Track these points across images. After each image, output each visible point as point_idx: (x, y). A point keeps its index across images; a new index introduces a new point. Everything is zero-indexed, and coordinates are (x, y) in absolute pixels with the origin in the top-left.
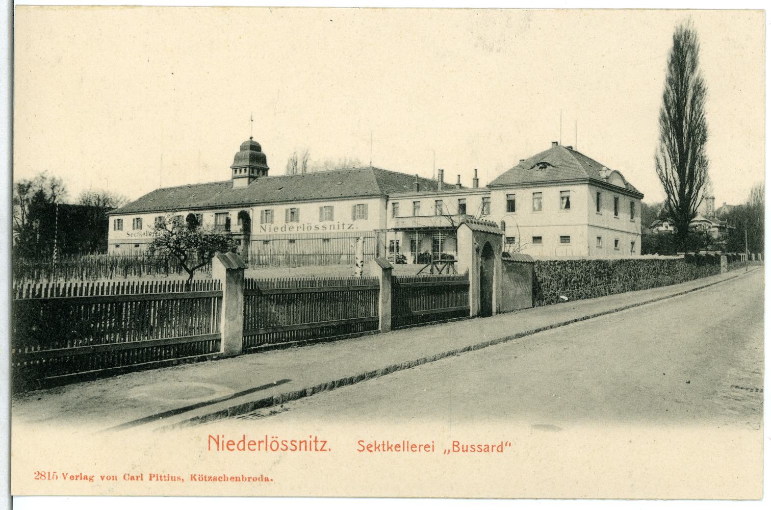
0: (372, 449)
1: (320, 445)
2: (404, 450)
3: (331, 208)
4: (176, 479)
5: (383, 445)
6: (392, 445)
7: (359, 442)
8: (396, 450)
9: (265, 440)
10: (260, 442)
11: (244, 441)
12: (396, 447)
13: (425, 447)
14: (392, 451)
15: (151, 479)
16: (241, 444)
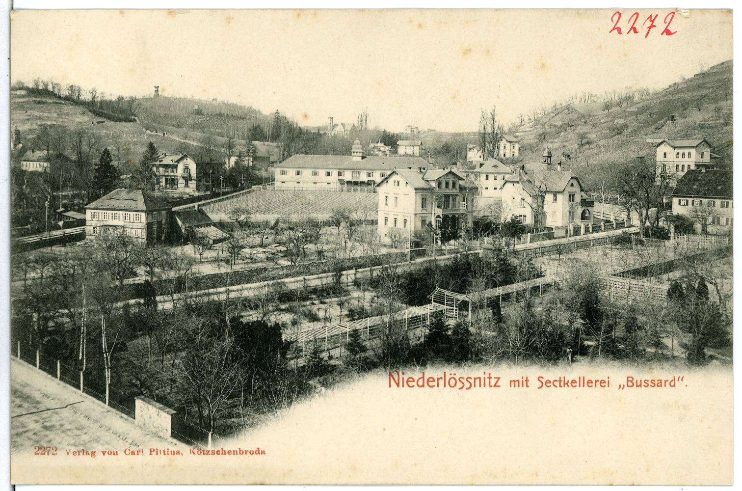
1: (493, 381)
2: (580, 386)
3: (714, 202)
4: (175, 453)
5: (560, 381)
6: (568, 381)
8: (572, 386)
9: (443, 378)
10: (438, 379)
11: (423, 378)
12: (572, 383)
13: (601, 383)
14: (568, 386)
15: (151, 454)
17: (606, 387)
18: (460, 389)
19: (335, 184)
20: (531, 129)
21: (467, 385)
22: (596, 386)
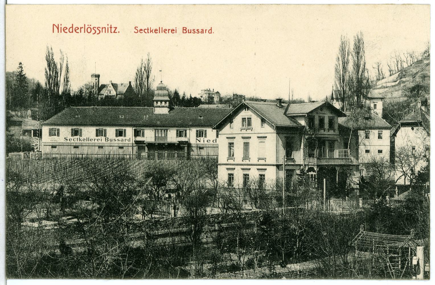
0: (67, 31)
1: (113, 30)
2: (159, 33)
3: (58, 130)
5: (148, 29)
7: (135, 27)
9: (84, 27)
10: (81, 28)
11: (72, 27)
12: (155, 31)
13: (172, 31)
16: (71, 29)
17: (158, 33)
18: (93, 34)
19: (130, 149)
20: (394, 84)
21: (98, 32)
22: (169, 33)
